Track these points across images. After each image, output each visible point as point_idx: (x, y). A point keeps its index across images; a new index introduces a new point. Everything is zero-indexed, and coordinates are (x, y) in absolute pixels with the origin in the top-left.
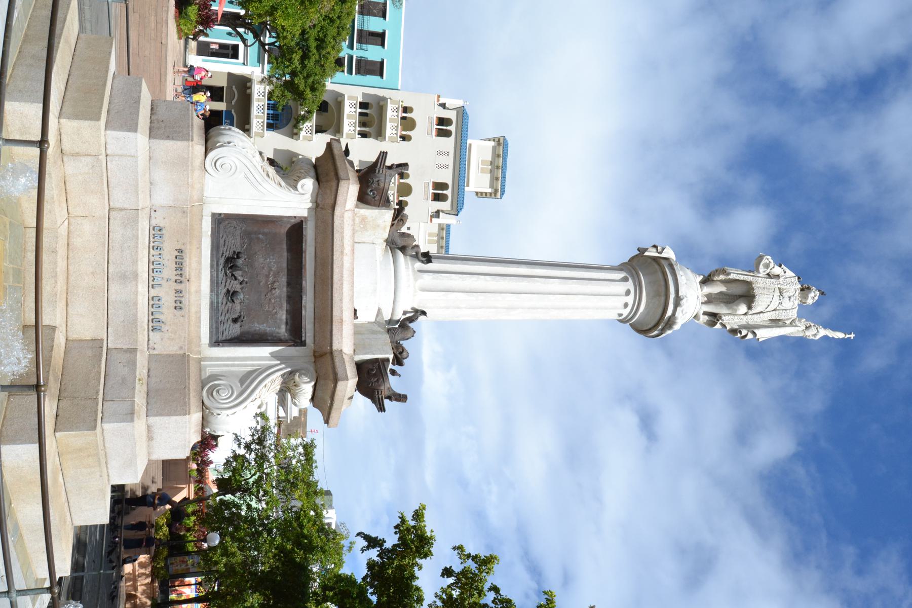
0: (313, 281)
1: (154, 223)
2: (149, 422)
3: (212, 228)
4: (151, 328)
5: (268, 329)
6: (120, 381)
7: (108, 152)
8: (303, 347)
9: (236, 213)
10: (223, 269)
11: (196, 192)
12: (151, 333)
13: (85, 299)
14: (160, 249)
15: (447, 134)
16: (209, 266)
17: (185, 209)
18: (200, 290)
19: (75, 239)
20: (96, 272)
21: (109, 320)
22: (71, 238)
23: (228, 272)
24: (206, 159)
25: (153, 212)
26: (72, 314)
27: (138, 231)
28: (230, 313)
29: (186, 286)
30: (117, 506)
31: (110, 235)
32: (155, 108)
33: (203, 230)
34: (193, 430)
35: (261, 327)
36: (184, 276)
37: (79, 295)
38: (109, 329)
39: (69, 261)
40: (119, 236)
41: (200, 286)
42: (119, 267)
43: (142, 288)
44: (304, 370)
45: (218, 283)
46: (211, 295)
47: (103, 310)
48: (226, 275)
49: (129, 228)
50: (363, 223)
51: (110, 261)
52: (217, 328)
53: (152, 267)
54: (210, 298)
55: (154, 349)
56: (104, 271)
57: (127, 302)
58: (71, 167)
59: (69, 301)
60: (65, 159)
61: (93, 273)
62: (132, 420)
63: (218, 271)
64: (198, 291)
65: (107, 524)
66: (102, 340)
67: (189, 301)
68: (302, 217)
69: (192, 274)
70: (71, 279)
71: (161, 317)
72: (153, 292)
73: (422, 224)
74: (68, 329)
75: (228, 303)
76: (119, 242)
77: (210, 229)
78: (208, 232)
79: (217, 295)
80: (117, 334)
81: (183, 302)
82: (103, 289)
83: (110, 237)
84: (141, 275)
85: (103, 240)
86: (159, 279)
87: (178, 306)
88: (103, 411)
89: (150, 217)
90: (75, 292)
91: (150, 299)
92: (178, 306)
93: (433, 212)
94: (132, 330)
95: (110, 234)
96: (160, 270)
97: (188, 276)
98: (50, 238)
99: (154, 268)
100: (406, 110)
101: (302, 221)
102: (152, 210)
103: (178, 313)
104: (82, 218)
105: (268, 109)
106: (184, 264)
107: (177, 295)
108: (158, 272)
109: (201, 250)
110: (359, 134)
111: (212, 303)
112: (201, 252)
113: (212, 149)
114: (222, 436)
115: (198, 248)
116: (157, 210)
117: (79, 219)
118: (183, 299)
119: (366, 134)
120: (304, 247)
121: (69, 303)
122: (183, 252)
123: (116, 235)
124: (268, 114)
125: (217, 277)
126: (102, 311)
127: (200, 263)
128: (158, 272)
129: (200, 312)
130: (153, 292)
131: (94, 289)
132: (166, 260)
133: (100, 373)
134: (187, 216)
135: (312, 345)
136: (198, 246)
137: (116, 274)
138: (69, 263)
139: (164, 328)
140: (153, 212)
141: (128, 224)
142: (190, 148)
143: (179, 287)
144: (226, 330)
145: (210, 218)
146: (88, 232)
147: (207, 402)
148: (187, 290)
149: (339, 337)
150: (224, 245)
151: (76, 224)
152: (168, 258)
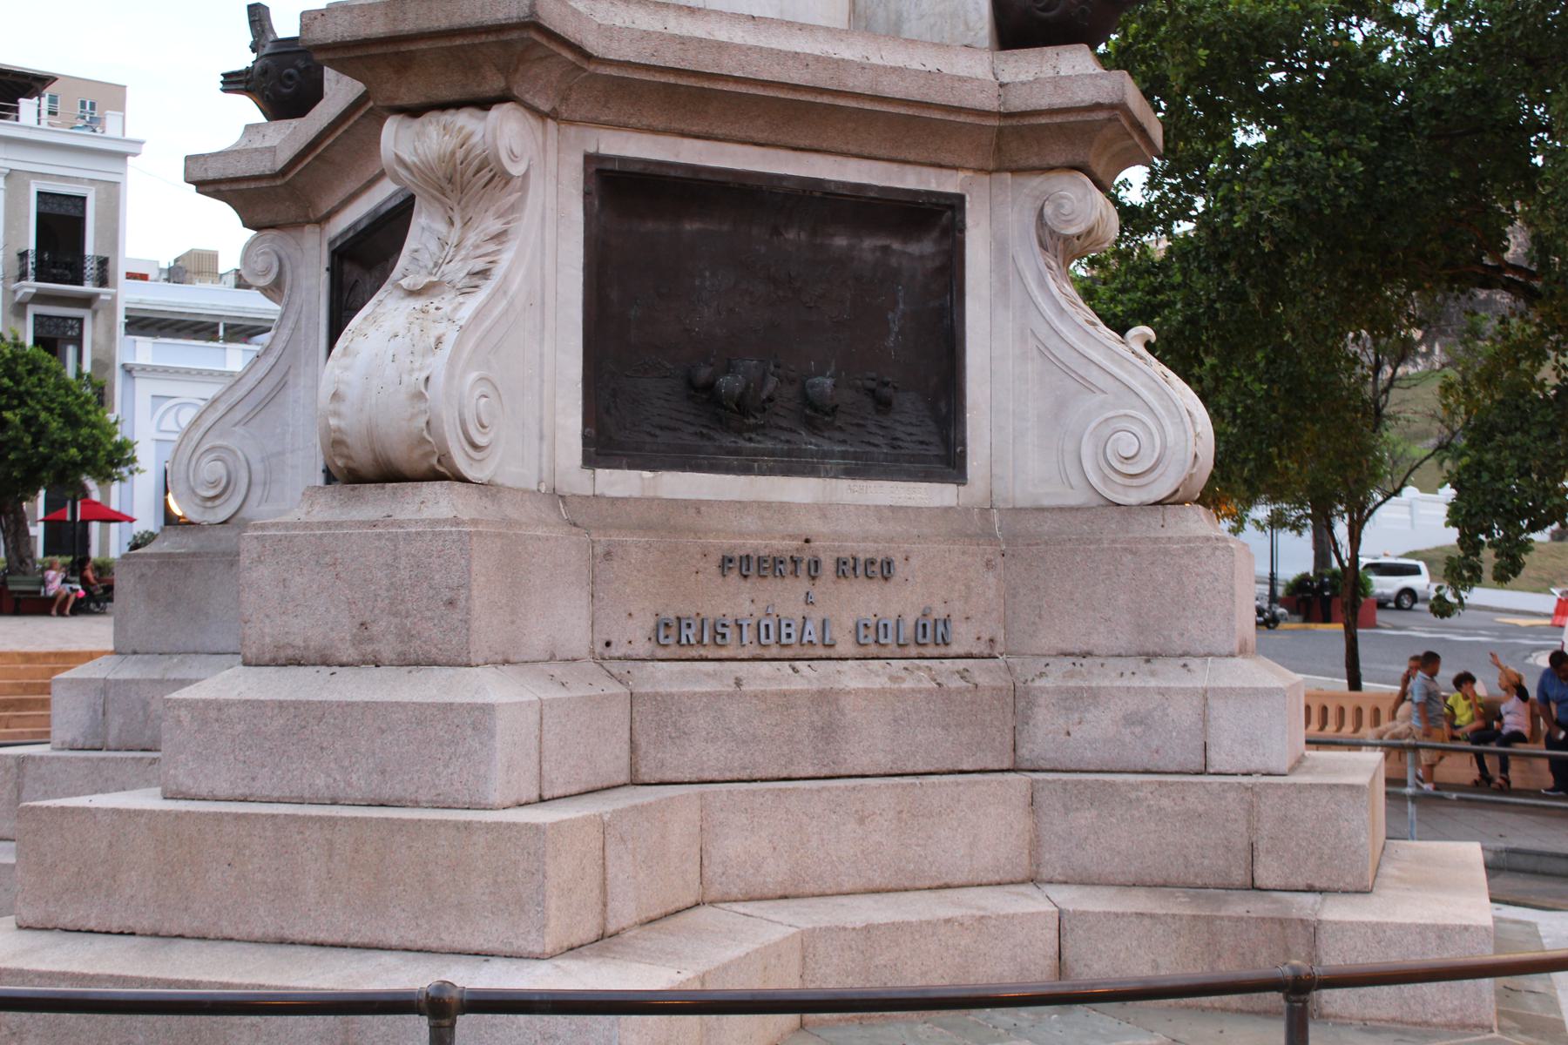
1: (643, 648)
3: (631, 467)
4: (942, 650)
5: (901, 306)
6: (1138, 730)
7: (534, 796)
8: (968, 205)
9: (580, 385)
10: (746, 435)
12: (955, 649)
13: (930, 837)
14: (724, 625)
16: (743, 478)
17: (599, 550)
19: (768, 879)
20: (857, 811)
21: (944, 769)
22: (766, 890)
23: (752, 421)
24: (470, 478)
25: (615, 651)
26: (970, 871)
27: (695, 694)
28: (863, 418)
31: (710, 778)
33: (636, 494)
35: (896, 329)
36: (796, 555)
37: (920, 856)
38: (965, 767)
39: (829, 892)
40: (711, 751)
41: (807, 507)
42: (800, 746)
44: (1041, 215)
45: (789, 454)
46: (827, 475)
47: (958, 784)
48: (763, 426)
49: (688, 722)
51: (784, 775)
52: (913, 458)
53: (774, 651)
54: (836, 477)
55: (992, 640)
56: (854, 788)
57: (895, 721)
58: (167, 925)
59: (937, 883)
60: (611, 928)
61: (861, 821)
63: (756, 452)
64: (823, 510)
66: (1033, 783)
68: (585, 170)
70: (878, 882)
71: (909, 621)
72: (845, 646)
74: (1008, 878)
75: (838, 423)
76: (729, 751)
77: (634, 473)
78: (642, 479)
79: (826, 455)
80: (979, 743)
81: (868, 556)
82: (904, 787)
83: (715, 775)
85: (767, 796)
86: (809, 627)
88: (1245, 771)
89: (627, 658)
90: (912, 866)
91: (861, 652)
94: (967, 703)
95: (706, 776)
96: (783, 626)
97: (795, 543)
98: (830, 949)
101: (599, 171)
102: (606, 656)
103: (899, 569)
104: (706, 862)
106: (762, 554)
107: (849, 573)
108: (789, 630)
109: (701, 501)
113: (444, 457)
116: (607, 638)
117: (708, 873)
118: (862, 557)
120: (679, 173)
121: (941, 882)
122: (729, 555)
123: (714, 758)
125: (772, 453)
126: (961, 788)
127: (741, 506)
128: (789, 630)
129: (878, 508)
130: (845, 646)
131: (904, 816)
132: (753, 607)
133: (238, 817)
134: (621, 544)
135: (961, 175)
136: (692, 511)
137: (820, 756)
138: (835, 889)
139: (939, 612)
140: (615, 651)
141: (674, 724)
143: (828, 565)
144: (911, 434)
145: (598, 471)
146: (748, 842)
147: (1161, 490)
148: (837, 544)
149: (968, 86)
150: (674, 429)
151: (724, 878)
152: (748, 603)
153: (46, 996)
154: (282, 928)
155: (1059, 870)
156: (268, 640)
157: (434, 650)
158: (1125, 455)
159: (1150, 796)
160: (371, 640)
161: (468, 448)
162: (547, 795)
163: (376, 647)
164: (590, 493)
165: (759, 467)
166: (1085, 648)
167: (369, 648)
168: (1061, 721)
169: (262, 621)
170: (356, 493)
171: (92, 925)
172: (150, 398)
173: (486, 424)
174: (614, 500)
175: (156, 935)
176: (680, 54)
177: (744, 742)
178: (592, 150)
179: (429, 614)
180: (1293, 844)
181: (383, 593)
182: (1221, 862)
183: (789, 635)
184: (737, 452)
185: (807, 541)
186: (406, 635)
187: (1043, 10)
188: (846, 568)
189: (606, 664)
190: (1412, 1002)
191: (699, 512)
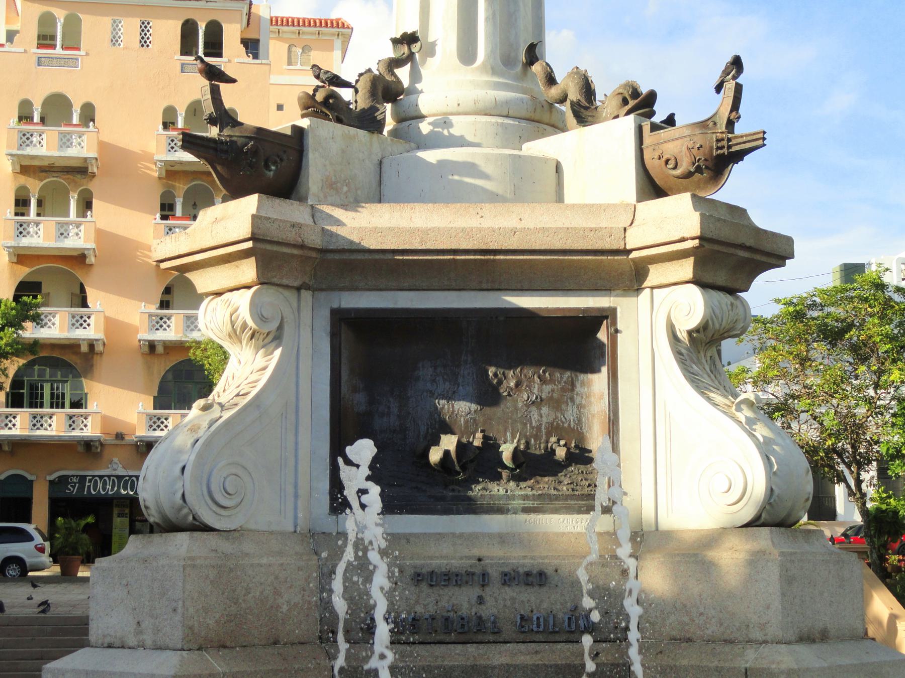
0: (473, 293)
2: (793, 638)
10: (451, 487)
11: (287, 548)
15: (73, 25)
16: (445, 517)
29: (492, 565)
32: (108, 640)
34: (807, 547)
50: (339, 185)
69: (466, 552)
73: (274, 79)
84: (472, 659)
93: (247, 53)
100: (25, 117)
105: (42, 407)
109: (410, 534)
110: (85, 216)
112: (417, 536)
114: (727, 476)
115: (408, 541)
119: (87, 202)
124: (52, 407)
127: (440, 537)
136: (403, 542)
142: (198, 562)
156: (100, 632)
158: (726, 488)
161: (215, 508)
163: (145, 637)
176: (380, 239)
178: (335, 306)
181: (147, 603)
184: (443, 499)
186: (157, 630)
187: (675, 168)
191: (408, 542)
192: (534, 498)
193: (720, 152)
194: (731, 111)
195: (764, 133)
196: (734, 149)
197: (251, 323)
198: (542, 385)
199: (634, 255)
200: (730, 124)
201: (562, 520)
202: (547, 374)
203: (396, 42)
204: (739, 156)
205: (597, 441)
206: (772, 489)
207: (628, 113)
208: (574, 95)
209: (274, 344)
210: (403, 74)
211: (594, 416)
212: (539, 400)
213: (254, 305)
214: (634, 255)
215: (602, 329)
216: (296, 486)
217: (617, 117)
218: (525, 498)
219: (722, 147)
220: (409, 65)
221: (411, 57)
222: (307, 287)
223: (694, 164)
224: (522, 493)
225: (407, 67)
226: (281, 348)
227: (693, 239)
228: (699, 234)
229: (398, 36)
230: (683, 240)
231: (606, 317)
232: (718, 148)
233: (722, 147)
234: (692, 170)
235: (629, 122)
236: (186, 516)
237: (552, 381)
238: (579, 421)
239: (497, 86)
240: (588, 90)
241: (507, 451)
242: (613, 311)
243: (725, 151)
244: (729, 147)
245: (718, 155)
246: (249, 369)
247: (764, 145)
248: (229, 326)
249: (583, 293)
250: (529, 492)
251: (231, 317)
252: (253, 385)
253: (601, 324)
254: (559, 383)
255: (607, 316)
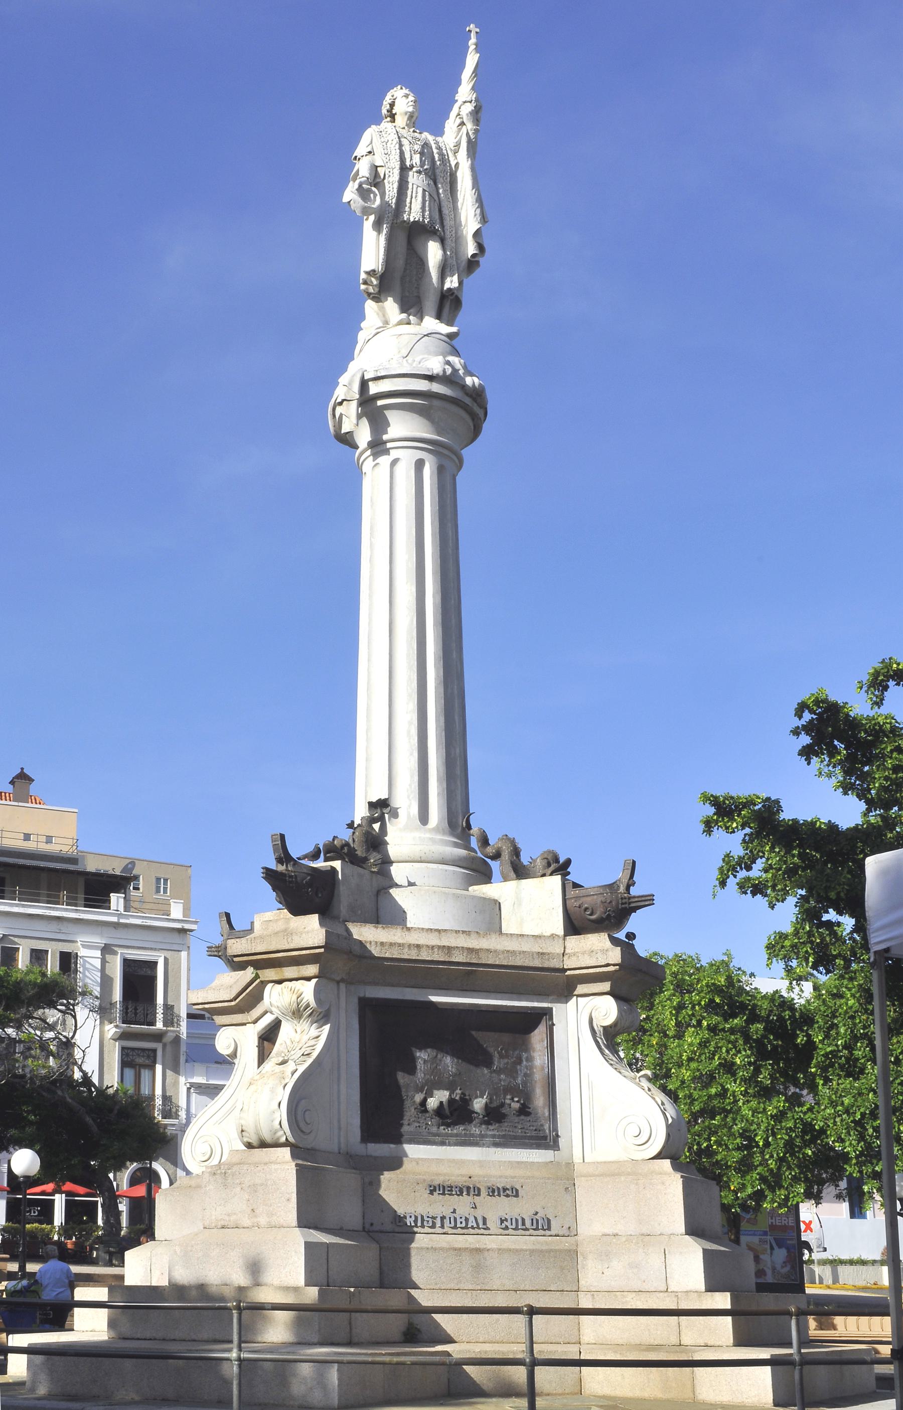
4: (548, 1233)
6: (635, 1270)
18: (480, 1162)
25: (375, 1228)
30: (56, 1247)
43: (489, 1242)
62: (299, 1227)
64: (481, 1164)
65: (121, 1278)
67: (501, 1177)
79: (482, 1136)
87: (511, 1192)
92: (511, 1192)
99: (463, 1226)
111: (496, 1145)
127: (439, 1161)
128: (461, 1220)
153: (128, 1221)
154: (215, 1335)
155: (592, 1338)
157: (282, 1221)
159: (632, 1300)
160: (256, 1216)
162: (355, 1340)
164: (365, 1154)
165: (449, 1142)
166: (615, 1232)
167: (255, 1220)
168: (600, 1267)
169: (211, 1209)
170: (251, 1153)
171: (139, 1336)
172: (631, 858)
173: (309, 1122)
174: (376, 1158)
175: (164, 1340)
177: (435, 1271)
178: (362, 995)
179: (280, 1205)
180: (697, 1323)
182: (665, 1332)
183: (461, 1223)
185: (470, 1177)
187: (591, 914)
188: (493, 1192)
189: (371, 1234)
190: (736, 1393)
192: (499, 1137)
193: (623, 906)
194: (630, 879)
195: (654, 896)
196: (632, 905)
197: (313, 1003)
198: (500, 1059)
199: (568, 973)
200: (628, 888)
201: (519, 1153)
202: (503, 1052)
203: (372, 805)
204: (634, 909)
205: (539, 1101)
206: (669, 1134)
207: (551, 874)
208: (506, 855)
209: (323, 1020)
210: (376, 826)
211: (536, 1082)
212: (498, 1069)
213: (317, 991)
214: (568, 973)
215: (542, 1022)
216: (339, 1121)
217: (544, 875)
218: (494, 1136)
219: (626, 903)
220: (379, 823)
221: (381, 819)
222: (342, 980)
223: (605, 913)
224: (491, 1133)
225: (379, 824)
226: (329, 1025)
227: (614, 965)
228: (620, 961)
229: (374, 800)
230: (608, 965)
231: (546, 1014)
232: (622, 904)
233: (626, 903)
234: (604, 917)
235: (557, 879)
236: (281, 1136)
237: (507, 1056)
238: (525, 1083)
239: (446, 843)
240: (516, 852)
241: (478, 1104)
242: (550, 1010)
243: (627, 905)
244: (630, 903)
245: (622, 908)
246: (305, 1038)
247: (654, 904)
248: (295, 1004)
249: (468, 993)
250: (495, 1132)
251: (298, 998)
252: (313, 1048)
253: (543, 1017)
254: (512, 1058)
255: (548, 1013)
